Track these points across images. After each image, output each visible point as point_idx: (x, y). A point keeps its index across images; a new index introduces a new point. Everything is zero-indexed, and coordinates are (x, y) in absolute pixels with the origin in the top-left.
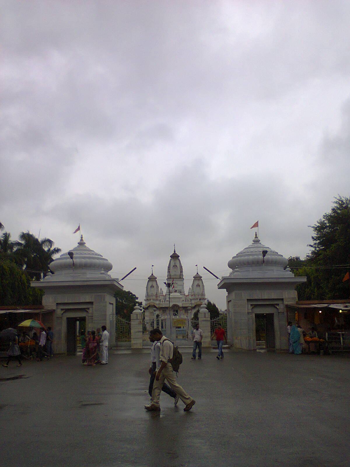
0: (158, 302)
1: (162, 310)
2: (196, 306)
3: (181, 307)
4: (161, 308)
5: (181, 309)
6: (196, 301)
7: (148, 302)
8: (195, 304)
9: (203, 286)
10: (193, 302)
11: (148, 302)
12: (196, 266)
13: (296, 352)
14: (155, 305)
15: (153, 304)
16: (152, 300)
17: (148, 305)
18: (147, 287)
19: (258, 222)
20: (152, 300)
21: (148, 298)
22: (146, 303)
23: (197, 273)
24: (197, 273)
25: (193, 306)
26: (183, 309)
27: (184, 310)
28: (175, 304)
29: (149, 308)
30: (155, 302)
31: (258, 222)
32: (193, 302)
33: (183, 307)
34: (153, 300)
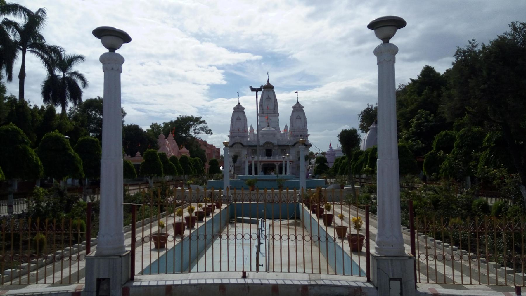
2: (295, 144)
3: (275, 146)
9: (305, 119)
12: (297, 93)
15: (239, 141)
20: (238, 137)
25: (293, 144)
33: (279, 146)
34: (239, 137)
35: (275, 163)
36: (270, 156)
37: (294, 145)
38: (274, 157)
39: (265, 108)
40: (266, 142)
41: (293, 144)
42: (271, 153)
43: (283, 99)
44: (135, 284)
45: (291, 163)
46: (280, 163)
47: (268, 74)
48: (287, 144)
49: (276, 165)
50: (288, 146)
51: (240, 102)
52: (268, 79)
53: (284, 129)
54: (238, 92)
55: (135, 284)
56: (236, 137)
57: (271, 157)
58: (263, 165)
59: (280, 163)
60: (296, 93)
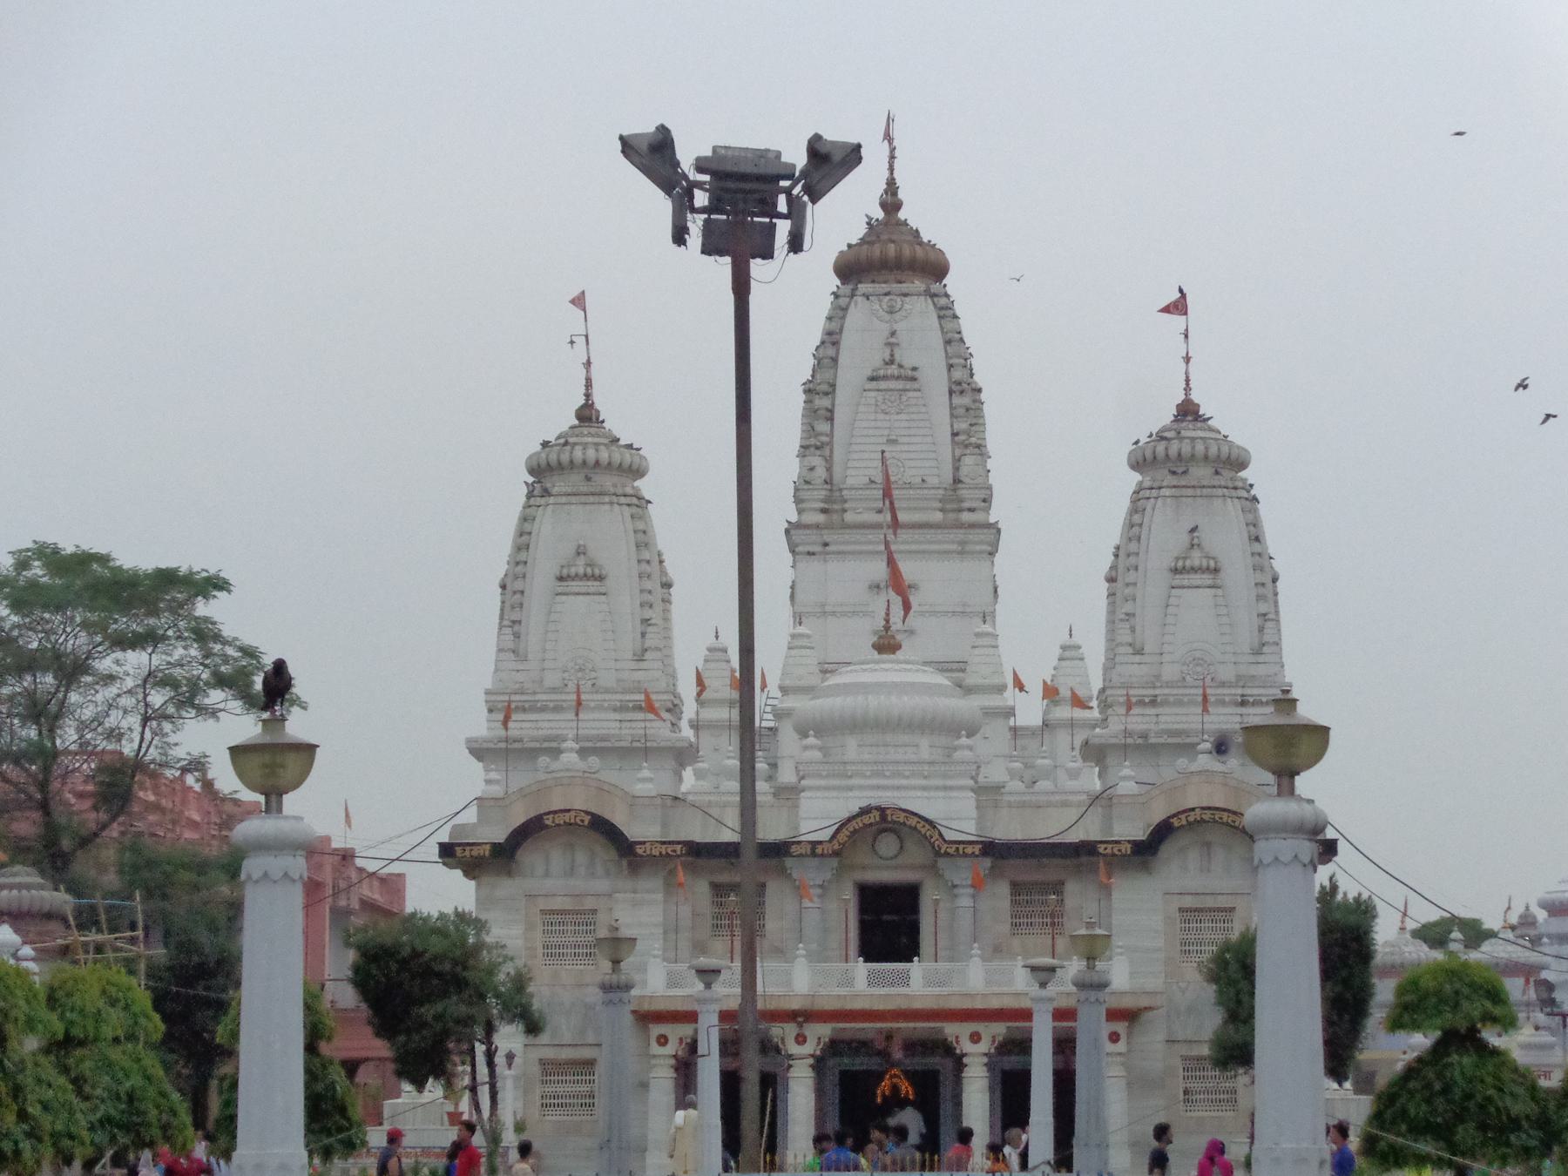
0: (646, 781)
1: (702, 888)
2: (1163, 831)
3: (958, 850)
4: (698, 851)
5: (961, 873)
6: (1169, 770)
7: (521, 778)
8: (1158, 815)
9: (1266, 582)
10: (1127, 778)
11: (521, 778)
12: (1177, 321)
13: (1265, 862)
14: (619, 819)
15: (580, 801)
16: (570, 758)
17: (519, 817)
18: (512, 589)
19: (583, 293)
20: (570, 758)
21: (521, 726)
22: (497, 791)
23: (587, 415)
24: (587, 415)
25: (1133, 829)
26: (994, 872)
27: (1003, 889)
28: (882, 810)
29: (528, 856)
30: (612, 774)
31: (583, 293)
32: (1127, 787)
33: (994, 850)
34: (583, 752)
35: (954, 1031)
36: (908, 959)
37: (1146, 850)
38: (943, 966)
39: (858, 470)
40: (865, 811)
41: (1141, 835)
42: (914, 930)
43: (838, 379)
44: (689, 215)
45: (1120, 1027)
46: (999, 1029)
47: (888, 137)
48: (1074, 837)
49: (966, 1046)
50: (1082, 852)
51: (599, 402)
52: (589, 383)
53: (1425, 948)
54: (579, 301)
55: (689, 215)
56: (556, 752)
57: (916, 970)
58: (834, 1047)
59: (999, 1029)
60: (1166, 310)
